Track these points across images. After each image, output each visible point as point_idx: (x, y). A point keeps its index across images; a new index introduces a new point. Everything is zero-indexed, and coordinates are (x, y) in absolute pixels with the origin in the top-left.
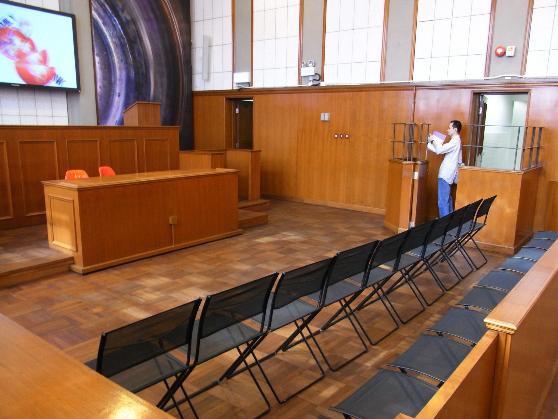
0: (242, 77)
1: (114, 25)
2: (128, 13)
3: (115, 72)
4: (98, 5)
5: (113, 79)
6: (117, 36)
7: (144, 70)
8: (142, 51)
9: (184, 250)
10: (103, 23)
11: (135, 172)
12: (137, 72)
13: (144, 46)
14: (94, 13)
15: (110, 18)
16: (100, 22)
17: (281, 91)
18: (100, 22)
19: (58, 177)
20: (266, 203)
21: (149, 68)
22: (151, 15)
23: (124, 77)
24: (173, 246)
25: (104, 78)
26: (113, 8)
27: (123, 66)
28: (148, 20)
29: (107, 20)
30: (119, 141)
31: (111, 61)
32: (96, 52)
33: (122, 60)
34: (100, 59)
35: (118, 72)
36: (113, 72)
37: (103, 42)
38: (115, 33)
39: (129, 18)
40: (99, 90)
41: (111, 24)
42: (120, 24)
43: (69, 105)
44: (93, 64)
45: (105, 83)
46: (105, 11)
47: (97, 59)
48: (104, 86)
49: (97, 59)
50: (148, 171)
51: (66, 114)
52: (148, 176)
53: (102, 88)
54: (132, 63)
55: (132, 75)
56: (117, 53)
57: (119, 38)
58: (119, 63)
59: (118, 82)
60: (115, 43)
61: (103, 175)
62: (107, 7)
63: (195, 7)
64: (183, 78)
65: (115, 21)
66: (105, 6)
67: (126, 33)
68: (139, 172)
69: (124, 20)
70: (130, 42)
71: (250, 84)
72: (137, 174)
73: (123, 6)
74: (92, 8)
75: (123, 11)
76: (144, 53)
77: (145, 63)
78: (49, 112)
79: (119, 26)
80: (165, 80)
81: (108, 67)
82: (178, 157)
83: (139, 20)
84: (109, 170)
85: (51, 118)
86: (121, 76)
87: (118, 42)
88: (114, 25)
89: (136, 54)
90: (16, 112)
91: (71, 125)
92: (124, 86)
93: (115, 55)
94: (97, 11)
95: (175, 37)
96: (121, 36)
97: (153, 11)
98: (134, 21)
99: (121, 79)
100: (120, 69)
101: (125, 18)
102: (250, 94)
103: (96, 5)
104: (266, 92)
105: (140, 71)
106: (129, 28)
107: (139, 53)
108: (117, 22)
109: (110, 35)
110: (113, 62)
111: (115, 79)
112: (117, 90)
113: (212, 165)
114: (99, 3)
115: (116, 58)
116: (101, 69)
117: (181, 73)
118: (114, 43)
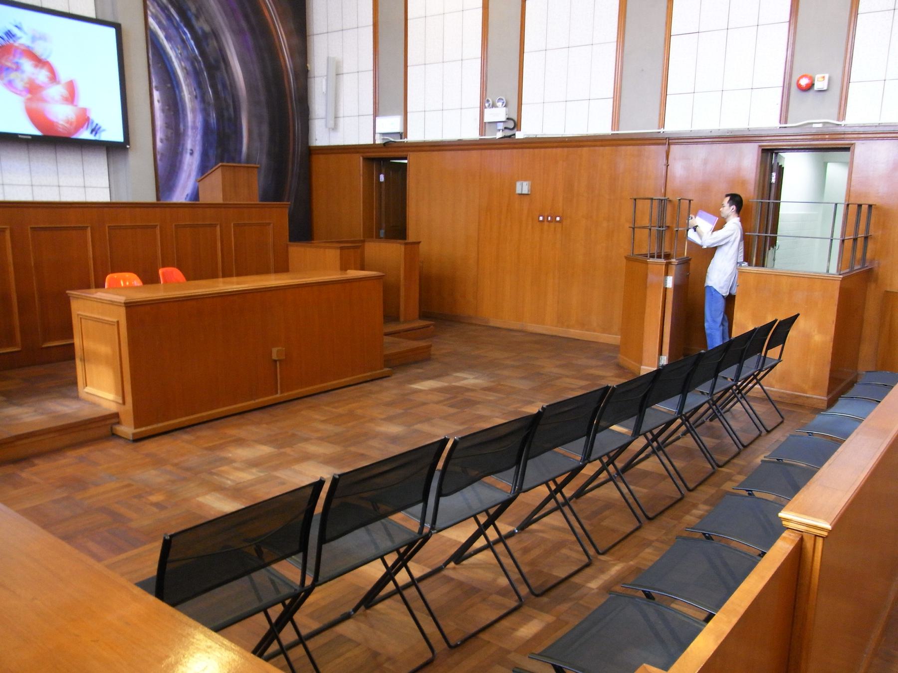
0: (390, 124)
1: (183, 41)
2: (207, 21)
3: (185, 115)
4: (158, 8)
5: (182, 126)
6: (188, 59)
7: (232, 113)
8: (228, 83)
9: (296, 402)
10: (166, 37)
11: (217, 277)
12: (220, 116)
13: (232, 74)
14: (151, 20)
15: (177, 28)
16: (161, 35)
17: (452, 145)
18: (161, 35)
19: (93, 284)
20: (428, 326)
21: (240, 108)
22: (244, 24)
23: (199, 124)
24: (278, 395)
25: (168, 126)
26: (182, 12)
27: (198, 105)
28: (238, 33)
29: (172, 31)
30: (191, 226)
31: (178, 98)
32: (154, 84)
33: (196, 97)
34: (161, 95)
35: (190, 116)
36: (181, 115)
37: (166, 67)
38: (185, 53)
39: (207, 28)
40: (159, 144)
41: (178, 39)
42: (193, 38)
43: (112, 169)
44: (150, 103)
45: (169, 134)
46: (169, 17)
47: (156, 95)
48: (167, 139)
49: (156, 95)
50: (239, 274)
51: (106, 183)
52: (238, 283)
53: (165, 141)
54: (212, 101)
55: (212, 121)
56: (188, 85)
57: (192, 60)
58: (191, 100)
59: (190, 132)
60: (185, 68)
61: (165, 281)
62: (172, 11)
63: (314, 11)
64: (294, 126)
65: (185, 33)
66: (169, 10)
67: (202, 53)
68: (224, 276)
69: (200, 32)
70: (209, 68)
71: (403, 134)
72: (221, 280)
73: (197, 10)
74: (149, 12)
75: (197, 18)
76: (231, 86)
77: (234, 102)
78: (79, 180)
79: (192, 42)
80: (265, 128)
81: (174, 107)
82: (287, 252)
83: (224, 33)
84: (176, 273)
85: (82, 190)
86: (194, 122)
87: (189, 68)
88: (183, 41)
89: (220, 87)
90: (26, 180)
91: (114, 200)
92: (199, 137)
93: (184, 88)
94: (155, 18)
95: (282, 60)
96: (195, 58)
97: (246, 17)
98: (215, 34)
99: (194, 128)
100: (193, 111)
101: (202, 29)
102: (403, 151)
103: (154, 8)
104: (428, 148)
105: (226, 114)
106: (208, 45)
107: (224, 86)
108: (189, 35)
109: (177, 57)
110: (182, 99)
111: (185, 126)
112: (189, 145)
113: (341, 264)
114: (159, 5)
115: (187, 93)
116: (163, 111)
117: (291, 117)
118: (184, 69)
